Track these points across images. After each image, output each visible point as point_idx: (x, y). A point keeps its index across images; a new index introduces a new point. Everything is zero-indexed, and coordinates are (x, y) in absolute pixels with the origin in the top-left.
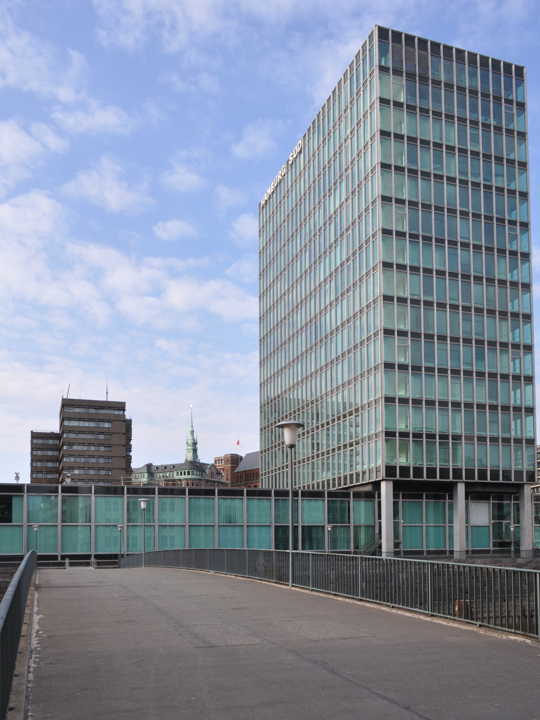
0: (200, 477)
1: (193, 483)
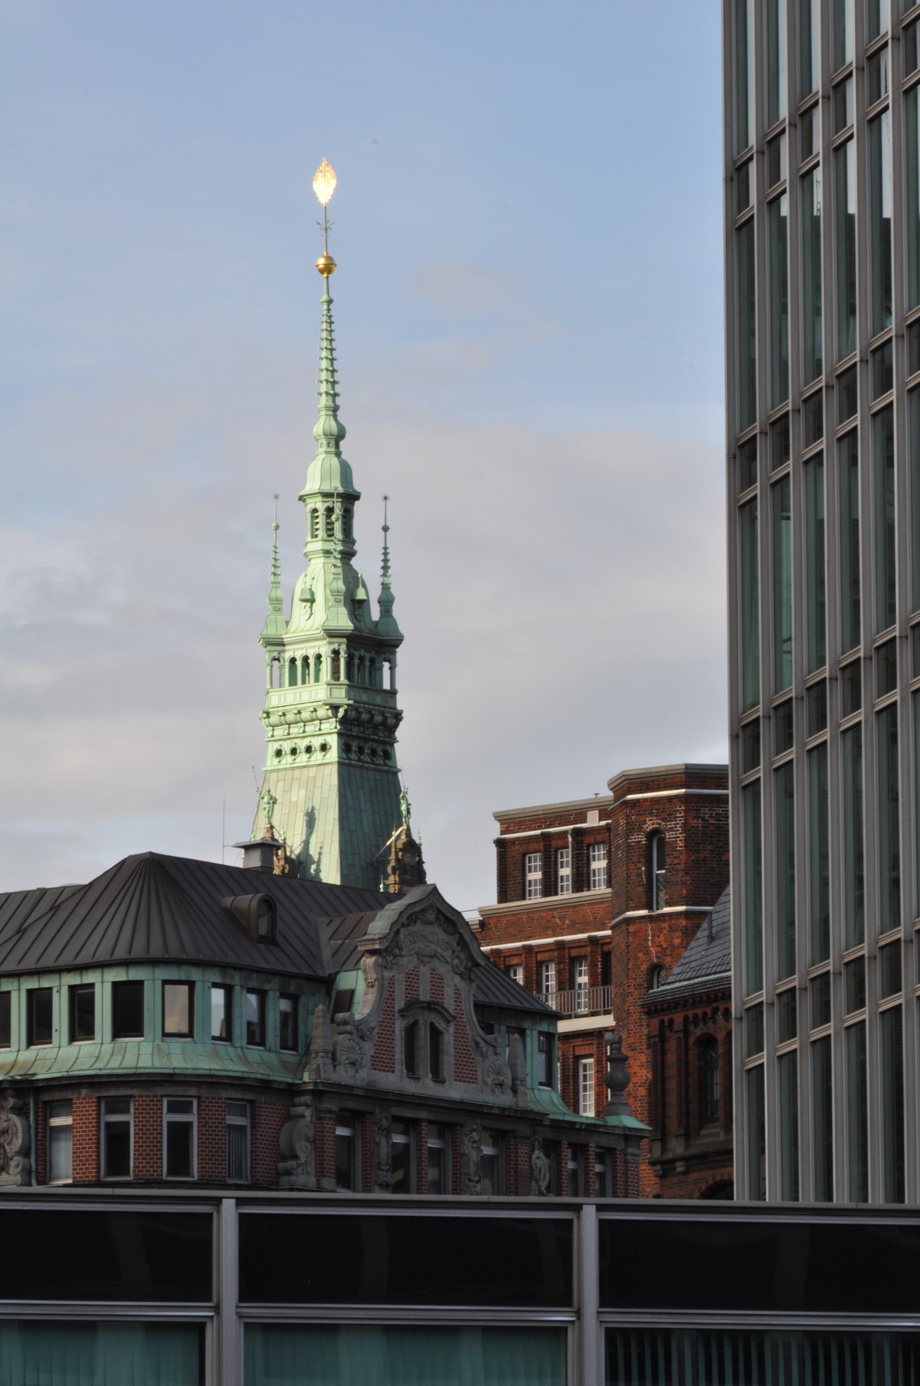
0: (260, 1062)
1: (179, 1133)
